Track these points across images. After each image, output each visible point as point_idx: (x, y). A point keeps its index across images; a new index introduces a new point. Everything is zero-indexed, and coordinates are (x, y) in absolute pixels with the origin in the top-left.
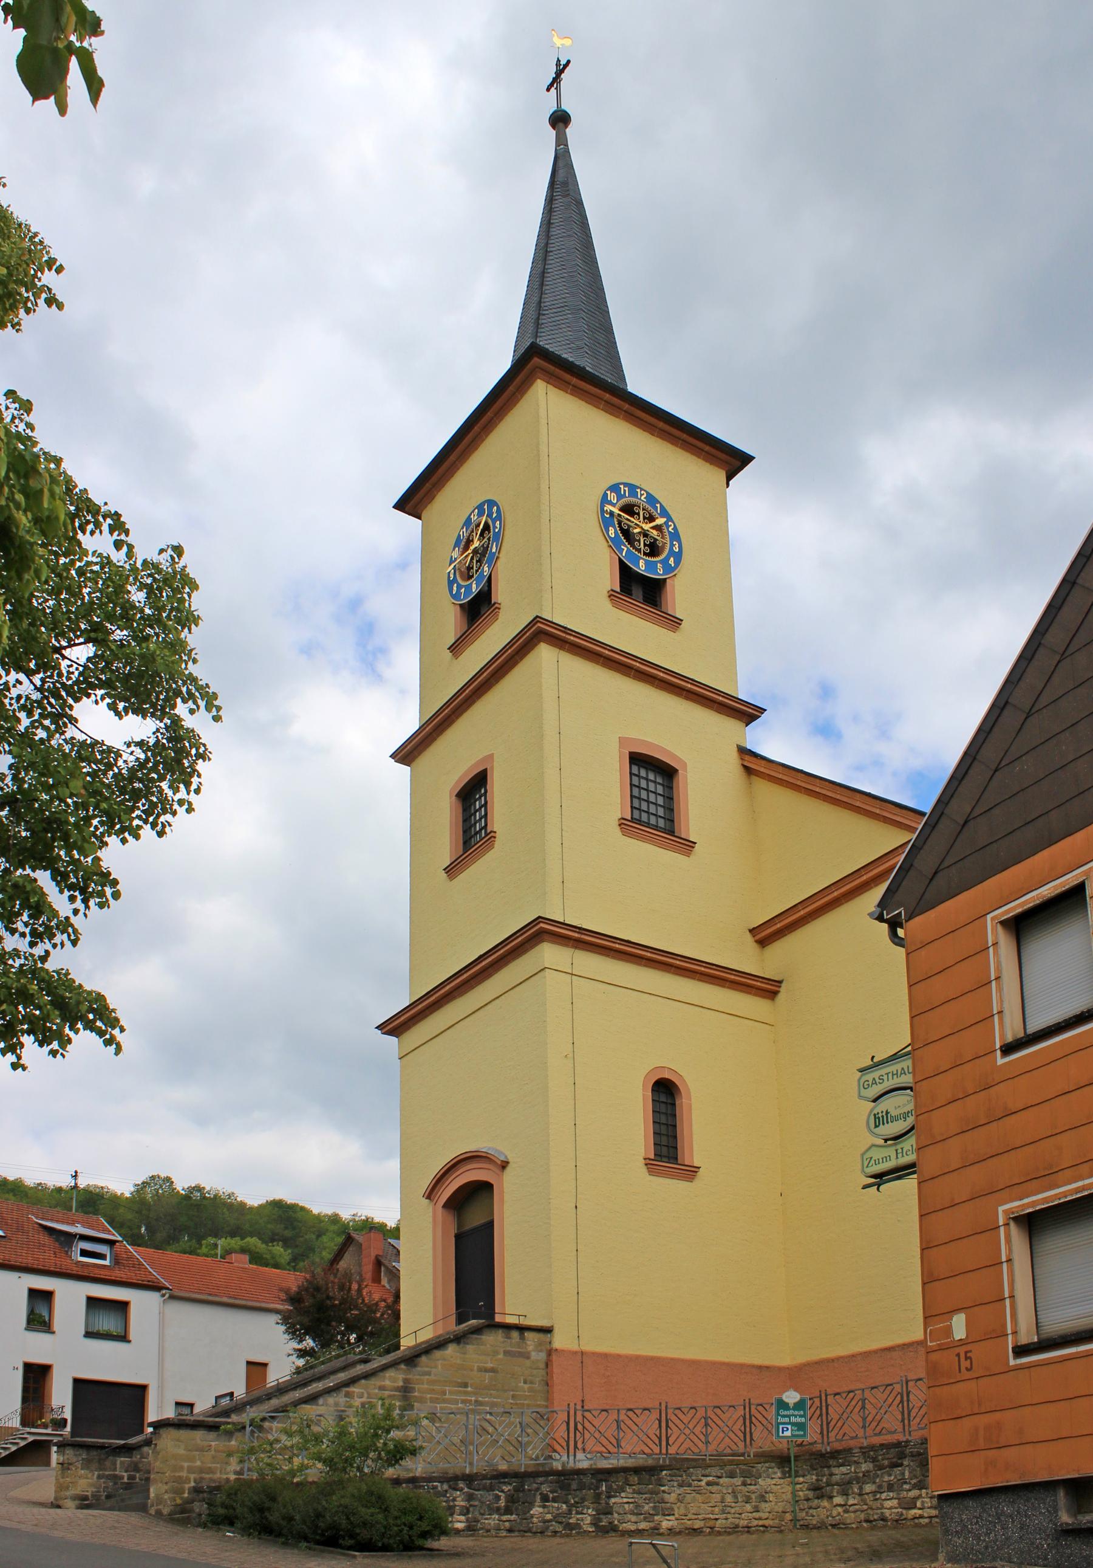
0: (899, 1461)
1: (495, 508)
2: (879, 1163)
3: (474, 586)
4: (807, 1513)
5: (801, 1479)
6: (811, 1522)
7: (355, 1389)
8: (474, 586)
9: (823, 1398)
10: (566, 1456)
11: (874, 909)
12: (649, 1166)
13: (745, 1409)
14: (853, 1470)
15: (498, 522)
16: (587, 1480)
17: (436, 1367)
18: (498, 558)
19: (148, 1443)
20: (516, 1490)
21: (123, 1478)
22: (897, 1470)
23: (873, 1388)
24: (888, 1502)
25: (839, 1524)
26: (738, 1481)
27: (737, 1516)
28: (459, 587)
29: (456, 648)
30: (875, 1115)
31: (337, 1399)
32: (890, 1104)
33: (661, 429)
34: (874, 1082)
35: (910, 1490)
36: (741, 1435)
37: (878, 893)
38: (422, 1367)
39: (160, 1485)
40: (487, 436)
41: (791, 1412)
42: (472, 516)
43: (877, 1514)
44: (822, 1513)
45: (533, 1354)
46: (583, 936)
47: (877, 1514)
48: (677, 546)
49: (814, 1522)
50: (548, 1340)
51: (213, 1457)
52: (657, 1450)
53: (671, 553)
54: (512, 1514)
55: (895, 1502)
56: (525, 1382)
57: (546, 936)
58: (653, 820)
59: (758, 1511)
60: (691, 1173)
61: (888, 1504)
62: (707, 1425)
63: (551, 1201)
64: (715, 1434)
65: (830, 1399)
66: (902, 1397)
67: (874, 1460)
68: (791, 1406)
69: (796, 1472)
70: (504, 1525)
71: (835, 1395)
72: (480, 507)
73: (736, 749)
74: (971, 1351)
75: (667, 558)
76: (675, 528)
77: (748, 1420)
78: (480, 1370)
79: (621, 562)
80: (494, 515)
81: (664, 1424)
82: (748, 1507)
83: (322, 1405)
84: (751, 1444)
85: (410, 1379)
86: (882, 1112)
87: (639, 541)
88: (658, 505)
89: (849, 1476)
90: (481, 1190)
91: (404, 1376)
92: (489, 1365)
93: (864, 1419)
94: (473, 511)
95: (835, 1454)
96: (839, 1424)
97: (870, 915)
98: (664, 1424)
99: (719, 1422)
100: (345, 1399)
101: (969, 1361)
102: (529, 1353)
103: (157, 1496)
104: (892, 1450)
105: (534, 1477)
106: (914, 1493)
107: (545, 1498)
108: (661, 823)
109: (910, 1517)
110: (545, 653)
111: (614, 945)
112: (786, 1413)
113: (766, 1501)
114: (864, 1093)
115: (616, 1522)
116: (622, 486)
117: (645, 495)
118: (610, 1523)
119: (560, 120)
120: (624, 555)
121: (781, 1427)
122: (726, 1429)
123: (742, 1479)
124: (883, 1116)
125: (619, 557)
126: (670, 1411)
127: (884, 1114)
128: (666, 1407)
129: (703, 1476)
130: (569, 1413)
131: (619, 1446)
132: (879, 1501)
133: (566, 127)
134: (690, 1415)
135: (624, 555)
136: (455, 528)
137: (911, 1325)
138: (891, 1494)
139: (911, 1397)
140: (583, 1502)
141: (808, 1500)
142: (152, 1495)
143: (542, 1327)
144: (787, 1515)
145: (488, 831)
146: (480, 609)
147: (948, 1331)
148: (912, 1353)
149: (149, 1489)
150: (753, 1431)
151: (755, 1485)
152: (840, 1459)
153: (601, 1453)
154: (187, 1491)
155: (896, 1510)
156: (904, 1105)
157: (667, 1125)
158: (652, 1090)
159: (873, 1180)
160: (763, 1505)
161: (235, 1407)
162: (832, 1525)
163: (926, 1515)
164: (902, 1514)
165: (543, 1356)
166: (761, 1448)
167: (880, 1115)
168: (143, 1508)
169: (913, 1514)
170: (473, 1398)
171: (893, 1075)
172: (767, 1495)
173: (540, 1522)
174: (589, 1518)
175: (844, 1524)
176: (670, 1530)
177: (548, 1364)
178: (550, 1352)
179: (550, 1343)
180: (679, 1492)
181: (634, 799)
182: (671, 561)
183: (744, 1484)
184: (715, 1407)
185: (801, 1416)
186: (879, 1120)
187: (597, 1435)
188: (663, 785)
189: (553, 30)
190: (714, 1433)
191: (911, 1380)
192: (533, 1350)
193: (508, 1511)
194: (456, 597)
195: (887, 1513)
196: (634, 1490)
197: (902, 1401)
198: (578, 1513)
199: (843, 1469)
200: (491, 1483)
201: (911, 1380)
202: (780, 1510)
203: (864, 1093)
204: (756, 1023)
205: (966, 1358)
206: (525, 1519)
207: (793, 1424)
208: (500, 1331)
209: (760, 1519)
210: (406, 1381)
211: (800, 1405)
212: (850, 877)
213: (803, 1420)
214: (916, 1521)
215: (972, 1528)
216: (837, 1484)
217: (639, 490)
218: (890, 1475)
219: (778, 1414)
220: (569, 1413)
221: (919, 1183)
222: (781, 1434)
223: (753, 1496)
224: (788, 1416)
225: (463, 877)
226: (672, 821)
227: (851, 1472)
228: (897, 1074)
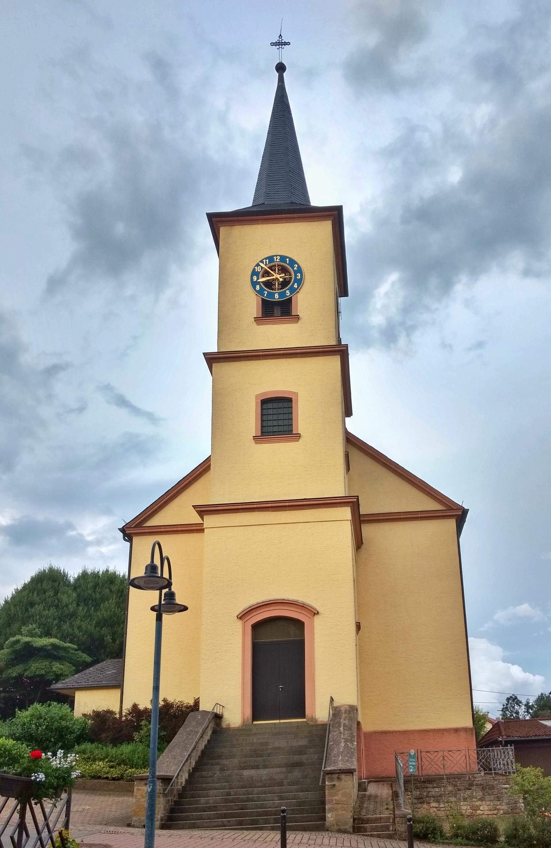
14: (442, 790)
23: (427, 752)
35: (477, 801)
42: (275, 258)
48: (299, 276)
94: (276, 256)
106: (479, 803)
133: (284, 72)
137: (438, 721)
138: (466, 803)
169: (479, 813)
182: (296, 286)
199: (437, 790)
216: (433, 797)
227: (442, 791)
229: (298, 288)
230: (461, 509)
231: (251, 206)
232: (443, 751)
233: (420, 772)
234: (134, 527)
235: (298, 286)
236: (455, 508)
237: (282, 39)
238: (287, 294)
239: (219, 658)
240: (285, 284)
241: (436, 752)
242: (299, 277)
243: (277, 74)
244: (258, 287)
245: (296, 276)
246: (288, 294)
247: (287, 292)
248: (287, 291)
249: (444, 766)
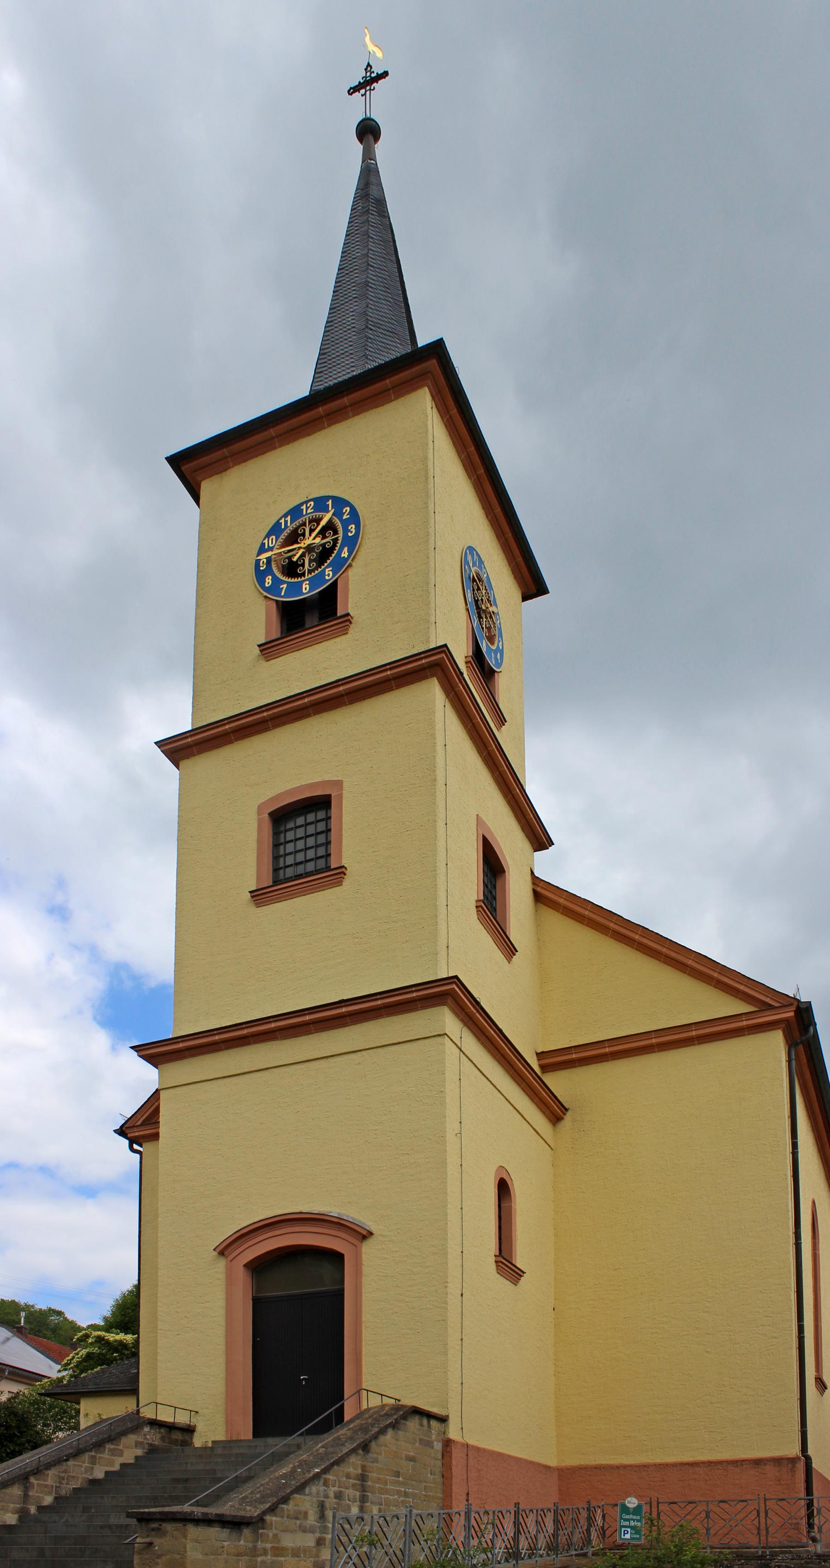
12: (500, 1264)
18: (350, 566)
38: (372, 1453)
40: (329, 425)
41: (631, 1516)
42: (304, 507)
46: (477, 1014)
57: (450, 1000)
63: (449, 1285)
68: (631, 1511)
83: (308, 1495)
94: (306, 502)
104: (752, 1562)
112: (627, 1517)
121: (623, 1529)
133: (375, 144)
146: (304, 620)
148: (720, 1471)
170: (403, 1489)
178: (448, 1443)
179: (444, 1433)
182: (345, 554)
185: (638, 1521)
189: (366, 28)
207: (632, 1528)
210: (363, 1467)
211: (637, 1510)
219: (621, 1518)
222: (623, 1537)
224: (628, 1520)
229: (349, 556)
230: (792, 1004)
231: (303, 391)
232: (707, 1503)
233: (763, 1538)
234: (141, 1125)
235: (350, 553)
236: (777, 1005)
237: (372, 70)
238: (327, 578)
239: (188, 1327)
240: (323, 555)
241: (690, 1503)
242: (352, 532)
243: (360, 147)
244: (269, 581)
245: (346, 530)
246: (329, 575)
247: (327, 573)
248: (327, 570)
249: (708, 1530)
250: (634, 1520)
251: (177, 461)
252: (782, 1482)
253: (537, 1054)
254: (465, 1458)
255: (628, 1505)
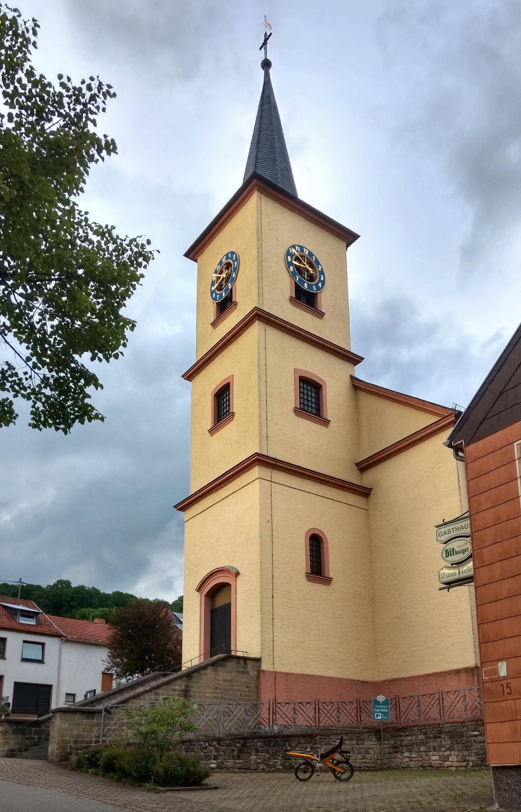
0: (439, 735)
1: (235, 255)
2: (449, 576)
3: (224, 293)
4: (390, 760)
5: (386, 742)
6: (392, 765)
7: (160, 691)
8: (224, 293)
9: (397, 699)
10: (268, 727)
11: (446, 441)
12: (308, 577)
13: (357, 703)
15: (236, 262)
16: (279, 740)
17: (202, 679)
18: (236, 280)
19: (49, 719)
20: (243, 746)
21: (35, 739)
22: (438, 740)
24: (433, 757)
25: (407, 767)
26: (354, 742)
27: (354, 761)
28: (216, 294)
29: (214, 324)
30: (446, 550)
31: (150, 696)
32: (455, 545)
33: (299, 210)
34: (445, 533)
35: (445, 751)
36: (356, 718)
37: (449, 431)
39: (54, 745)
41: (381, 706)
43: (427, 763)
44: (398, 761)
45: (251, 672)
46: (277, 463)
47: (427, 763)
48: (323, 277)
49: (394, 766)
50: (259, 665)
51: (84, 729)
52: (313, 724)
53: (320, 280)
54: (240, 760)
55: (437, 757)
56: (247, 687)
58: (310, 409)
59: (364, 759)
60: (328, 581)
61: (433, 758)
62: (338, 712)
64: (343, 717)
65: (401, 700)
66: (439, 701)
67: (425, 734)
68: (381, 703)
69: (384, 738)
70: (236, 765)
71: (404, 698)
72: (227, 255)
73: (349, 377)
74: (510, 683)
75: (318, 283)
76: (322, 269)
77: (359, 710)
78: (224, 681)
79: (296, 284)
80: (234, 259)
81: (317, 711)
82: (360, 756)
84: (360, 723)
85: (188, 685)
86: (450, 549)
87: (305, 274)
88: (314, 257)
89: (411, 741)
90: (224, 587)
91: (185, 684)
92: (229, 678)
93: (419, 711)
94: (223, 257)
95: (403, 729)
96: (406, 714)
97: (444, 444)
98: (317, 711)
99: (345, 711)
100: (155, 696)
101: (509, 689)
102: (249, 672)
103: (52, 751)
105: (252, 739)
107: (257, 751)
108: (314, 411)
109: (445, 766)
110: (257, 327)
111: (292, 468)
112: (378, 707)
113: (369, 753)
114: (439, 538)
115: (293, 764)
116: (297, 247)
117: (308, 252)
118: (290, 764)
119: (266, 64)
120: (297, 280)
121: (376, 714)
122: (348, 714)
123: (356, 741)
124: (451, 551)
125: (295, 282)
126: (320, 704)
127: (451, 550)
128: (318, 702)
129: (337, 739)
130: (269, 704)
131: (295, 722)
132: (429, 756)
134: (330, 706)
135: (297, 280)
136: (215, 265)
138: (435, 753)
139: (445, 701)
140: (276, 753)
141: (390, 753)
142: (50, 750)
143: (256, 658)
144: (379, 761)
145: (230, 412)
147: (496, 671)
149: (48, 746)
150: (361, 715)
151: (363, 744)
152: (407, 732)
153: (285, 725)
154: (69, 748)
155: (438, 762)
156: (463, 545)
157: (316, 557)
158: (310, 539)
159: (445, 586)
160: (367, 756)
161: (96, 699)
162: (402, 768)
163: (454, 765)
164: (441, 764)
165: (255, 673)
166: (365, 725)
167: (449, 551)
168: (45, 758)
171: (456, 529)
172: (369, 750)
173: (255, 763)
174: (280, 761)
175: (410, 768)
176: (321, 768)
177: (258, 677)
179: (259, 667)
180: (325, 748)
181: (301, 399)
182: (320, 285)
183: (358, 744)
184: (342, 702)
185: (386, 709)
186: (448, 553)
187: (284, 717)
188: (315, 393)
190: (342, 717)
191: (444, 692)
192: (251, 671)
193: (239, 758)
194: (214, 299)
195: (433, 763)
196: (303, 746)
197: (439, 703)
198: (274, 759)
199: (409, 738)
200: (230, 742)
201: (444, 692)
202: (376, 758)
203: (439, 538)
204: (359, 509)
205: (507, 687)
206: (247, 762)
207: (382, 713)
208: (235, 660)
209: (366, 763)
210: (187, 686)
211: (384, 703)
212: (409, 437)
213: (387, 711)
214: (449, 768)
215: (515, 788)
217: (305, 249)
218: (434, 742)
220: (269, 704)
221: (476, 588)
222: (376, 718)
223: (362, 751)
224: (380, 708)
225: (217, 435)
226: (319, 410)
227: (413, 739)
228: (458, 529)
250: (383, 709)
251: (187, 255)
252: (469, 682)
253: (356, 464)
254: (274, 679)
255: (379, 700)
